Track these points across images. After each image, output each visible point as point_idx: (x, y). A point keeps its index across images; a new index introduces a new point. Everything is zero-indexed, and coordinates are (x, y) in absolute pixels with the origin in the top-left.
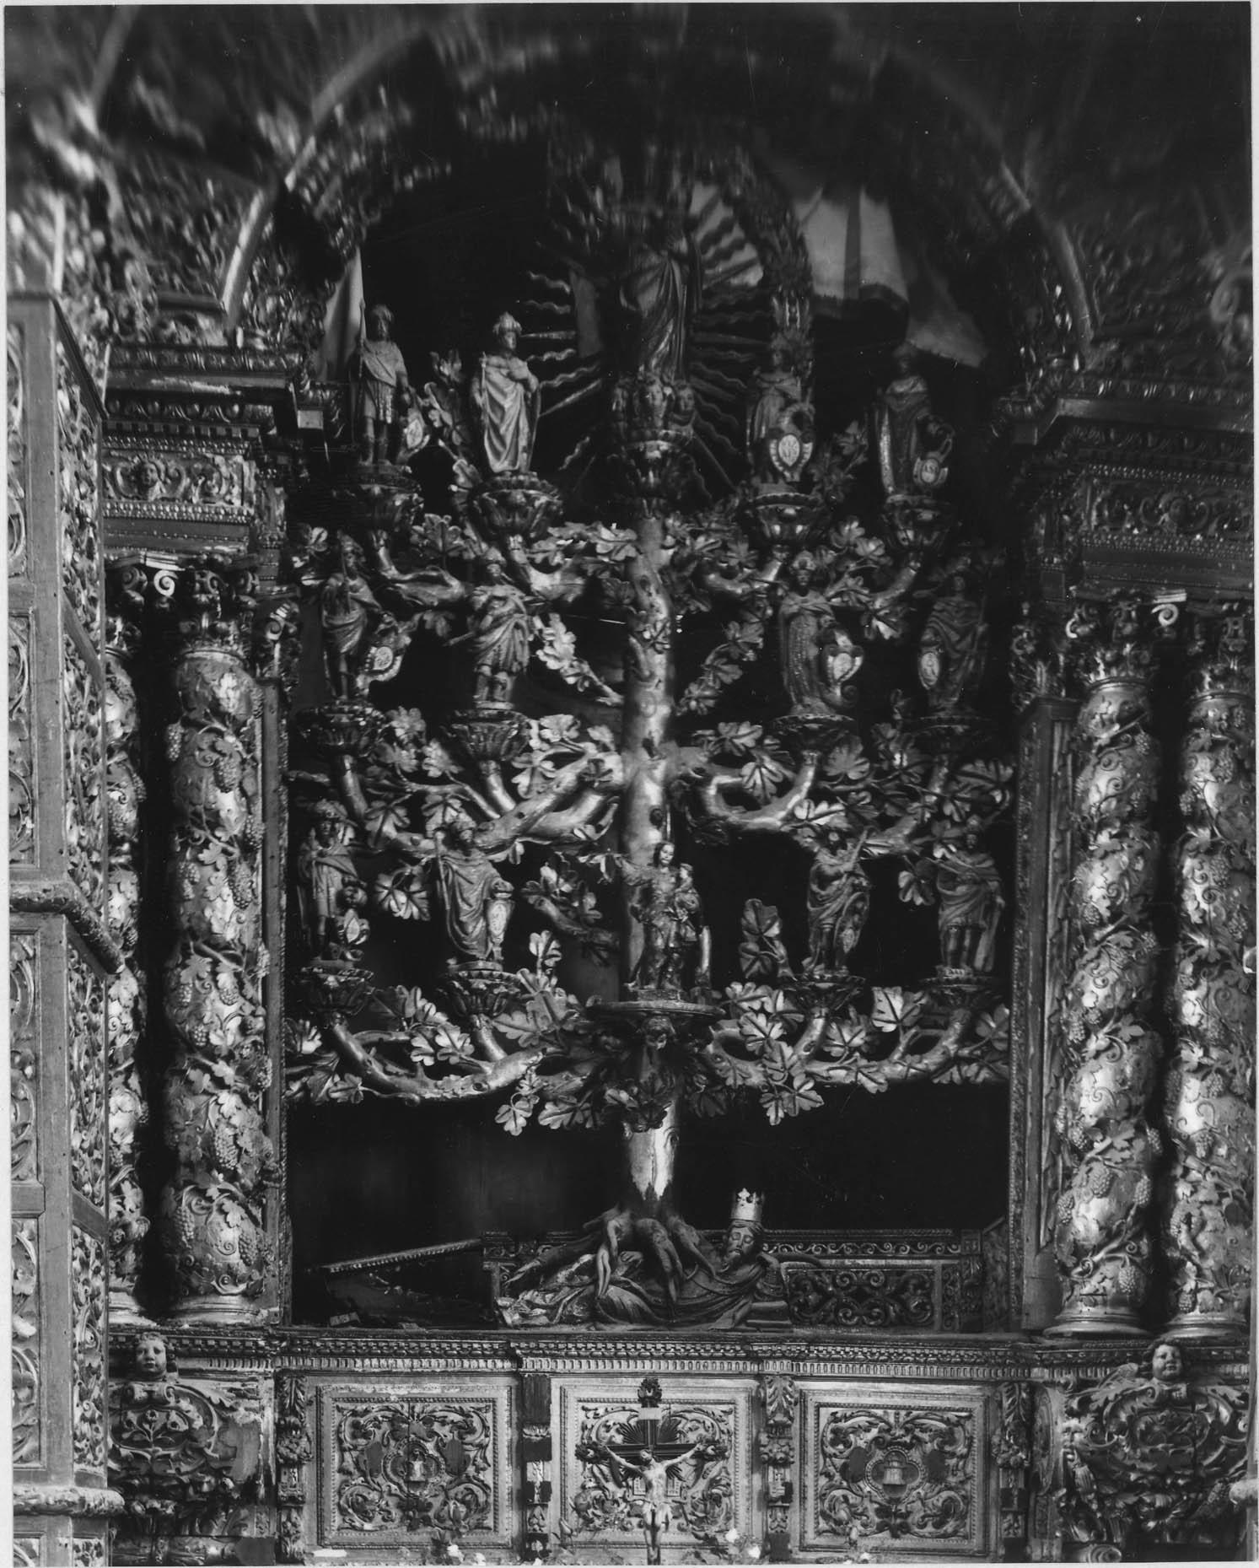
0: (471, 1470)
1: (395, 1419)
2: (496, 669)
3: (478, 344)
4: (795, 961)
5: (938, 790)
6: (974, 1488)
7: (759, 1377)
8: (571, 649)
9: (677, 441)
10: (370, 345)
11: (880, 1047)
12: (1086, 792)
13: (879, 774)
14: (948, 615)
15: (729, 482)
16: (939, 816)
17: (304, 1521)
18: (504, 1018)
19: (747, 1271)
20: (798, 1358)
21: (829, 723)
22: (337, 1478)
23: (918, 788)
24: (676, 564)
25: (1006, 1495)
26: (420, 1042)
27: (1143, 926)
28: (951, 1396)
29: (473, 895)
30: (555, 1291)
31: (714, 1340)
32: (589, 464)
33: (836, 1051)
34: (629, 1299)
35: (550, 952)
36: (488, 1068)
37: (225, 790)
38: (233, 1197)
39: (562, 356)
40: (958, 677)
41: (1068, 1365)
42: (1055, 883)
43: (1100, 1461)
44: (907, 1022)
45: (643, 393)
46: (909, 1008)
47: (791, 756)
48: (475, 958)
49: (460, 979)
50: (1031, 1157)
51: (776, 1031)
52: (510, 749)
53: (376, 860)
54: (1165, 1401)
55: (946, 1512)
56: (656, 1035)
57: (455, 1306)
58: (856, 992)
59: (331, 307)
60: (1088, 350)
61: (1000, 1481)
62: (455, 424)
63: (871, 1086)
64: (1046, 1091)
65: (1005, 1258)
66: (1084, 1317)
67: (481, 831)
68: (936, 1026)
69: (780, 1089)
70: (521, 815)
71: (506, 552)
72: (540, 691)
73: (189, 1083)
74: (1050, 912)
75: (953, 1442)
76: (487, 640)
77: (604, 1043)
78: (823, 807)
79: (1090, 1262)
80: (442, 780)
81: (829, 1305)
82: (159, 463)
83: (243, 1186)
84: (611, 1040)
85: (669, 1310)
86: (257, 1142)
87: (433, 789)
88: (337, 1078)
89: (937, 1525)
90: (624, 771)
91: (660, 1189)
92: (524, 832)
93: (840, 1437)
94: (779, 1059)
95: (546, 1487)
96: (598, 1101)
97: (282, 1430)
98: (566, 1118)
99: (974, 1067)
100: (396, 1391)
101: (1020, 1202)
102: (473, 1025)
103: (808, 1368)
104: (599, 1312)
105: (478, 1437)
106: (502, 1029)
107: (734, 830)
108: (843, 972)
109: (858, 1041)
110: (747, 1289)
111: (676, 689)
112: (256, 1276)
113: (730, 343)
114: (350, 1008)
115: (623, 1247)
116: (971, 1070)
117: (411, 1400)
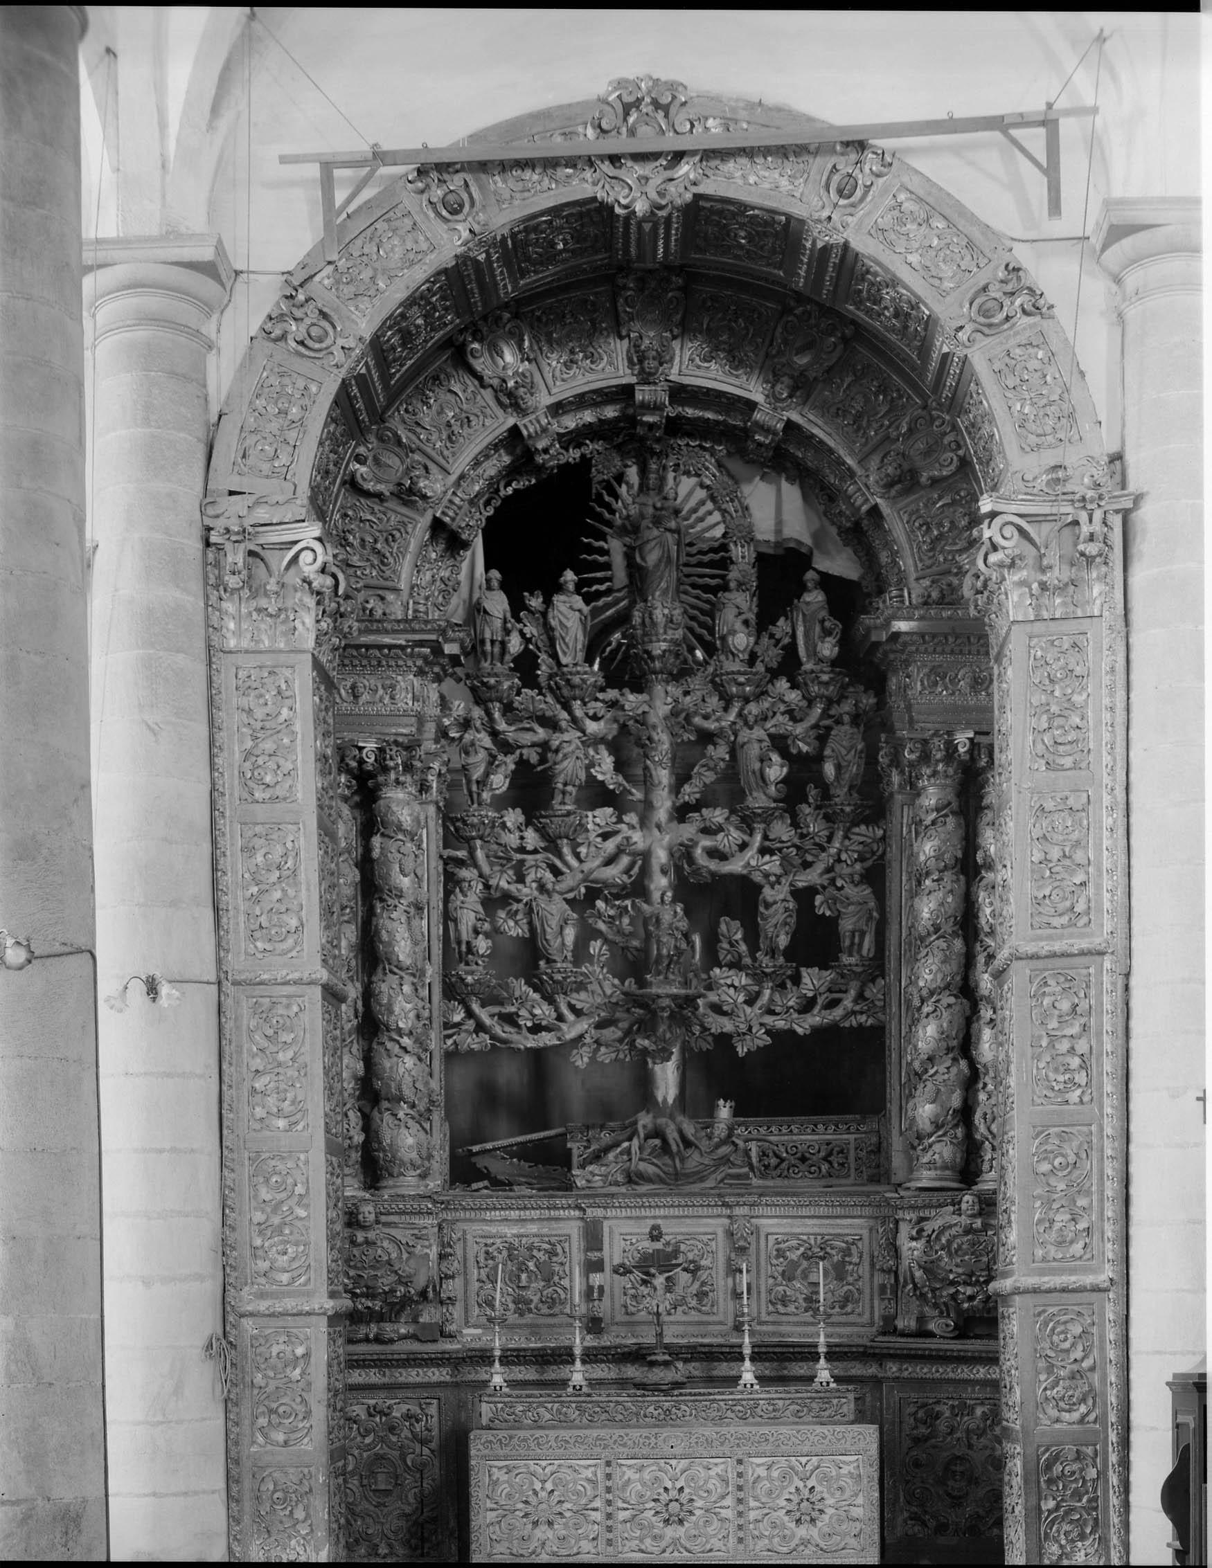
0: (556, 1278)
1: (511, 1248)
2: (565, 784)
3: (552, 588)
7: (729, 1217)
8: (611, 766)
9: (674, 642)
11: (807, 1006)
13: (802, 836)
16: (839, 861)
17: (457, 1311)
18: (575, 995)
22: (477, 1285)
24: (674, 713)
26: (523, 1012)
28: (853, 1226)
29: (554, 923)
31: (701, 1195)
33: (778, 1009)
36: (564, 1026)
41: (913, 1208)
43: (929, 1269)
45: (651, 614)
47: (747, 823)
51: (741, 999)
53: (495, 901)
54: (969, 1231)
55: (846, 1299)
57: (549, 1166)
59: (465, 566)
60: (913, 584)
61: (879, 1279)
63: (800, 1031)
66: (926, 1178)
68: (840, 991)
71: (570, 713)
72: (597, 795)
75: (850, 1255)
78: (767, 858)
79: (926, 1142)
80: (535, 851)
81: (784, 1165)
86: (427, 1083)
89: (842, 1307)
91: (670, 1101)
92: (585, 880)
95: (601, 1288)
97: (442, 1257)
98: (613, 1055)
103: (759, 1211)
104: (633, 1178)
105: (560, 1259)
107: (713, 874)
108: (781, 960)
109: (791, 1003)
110: (725, 1160)
111: (676, 789)
113: (708, 569)
115: (647, 1138)
117: (520, 1236)
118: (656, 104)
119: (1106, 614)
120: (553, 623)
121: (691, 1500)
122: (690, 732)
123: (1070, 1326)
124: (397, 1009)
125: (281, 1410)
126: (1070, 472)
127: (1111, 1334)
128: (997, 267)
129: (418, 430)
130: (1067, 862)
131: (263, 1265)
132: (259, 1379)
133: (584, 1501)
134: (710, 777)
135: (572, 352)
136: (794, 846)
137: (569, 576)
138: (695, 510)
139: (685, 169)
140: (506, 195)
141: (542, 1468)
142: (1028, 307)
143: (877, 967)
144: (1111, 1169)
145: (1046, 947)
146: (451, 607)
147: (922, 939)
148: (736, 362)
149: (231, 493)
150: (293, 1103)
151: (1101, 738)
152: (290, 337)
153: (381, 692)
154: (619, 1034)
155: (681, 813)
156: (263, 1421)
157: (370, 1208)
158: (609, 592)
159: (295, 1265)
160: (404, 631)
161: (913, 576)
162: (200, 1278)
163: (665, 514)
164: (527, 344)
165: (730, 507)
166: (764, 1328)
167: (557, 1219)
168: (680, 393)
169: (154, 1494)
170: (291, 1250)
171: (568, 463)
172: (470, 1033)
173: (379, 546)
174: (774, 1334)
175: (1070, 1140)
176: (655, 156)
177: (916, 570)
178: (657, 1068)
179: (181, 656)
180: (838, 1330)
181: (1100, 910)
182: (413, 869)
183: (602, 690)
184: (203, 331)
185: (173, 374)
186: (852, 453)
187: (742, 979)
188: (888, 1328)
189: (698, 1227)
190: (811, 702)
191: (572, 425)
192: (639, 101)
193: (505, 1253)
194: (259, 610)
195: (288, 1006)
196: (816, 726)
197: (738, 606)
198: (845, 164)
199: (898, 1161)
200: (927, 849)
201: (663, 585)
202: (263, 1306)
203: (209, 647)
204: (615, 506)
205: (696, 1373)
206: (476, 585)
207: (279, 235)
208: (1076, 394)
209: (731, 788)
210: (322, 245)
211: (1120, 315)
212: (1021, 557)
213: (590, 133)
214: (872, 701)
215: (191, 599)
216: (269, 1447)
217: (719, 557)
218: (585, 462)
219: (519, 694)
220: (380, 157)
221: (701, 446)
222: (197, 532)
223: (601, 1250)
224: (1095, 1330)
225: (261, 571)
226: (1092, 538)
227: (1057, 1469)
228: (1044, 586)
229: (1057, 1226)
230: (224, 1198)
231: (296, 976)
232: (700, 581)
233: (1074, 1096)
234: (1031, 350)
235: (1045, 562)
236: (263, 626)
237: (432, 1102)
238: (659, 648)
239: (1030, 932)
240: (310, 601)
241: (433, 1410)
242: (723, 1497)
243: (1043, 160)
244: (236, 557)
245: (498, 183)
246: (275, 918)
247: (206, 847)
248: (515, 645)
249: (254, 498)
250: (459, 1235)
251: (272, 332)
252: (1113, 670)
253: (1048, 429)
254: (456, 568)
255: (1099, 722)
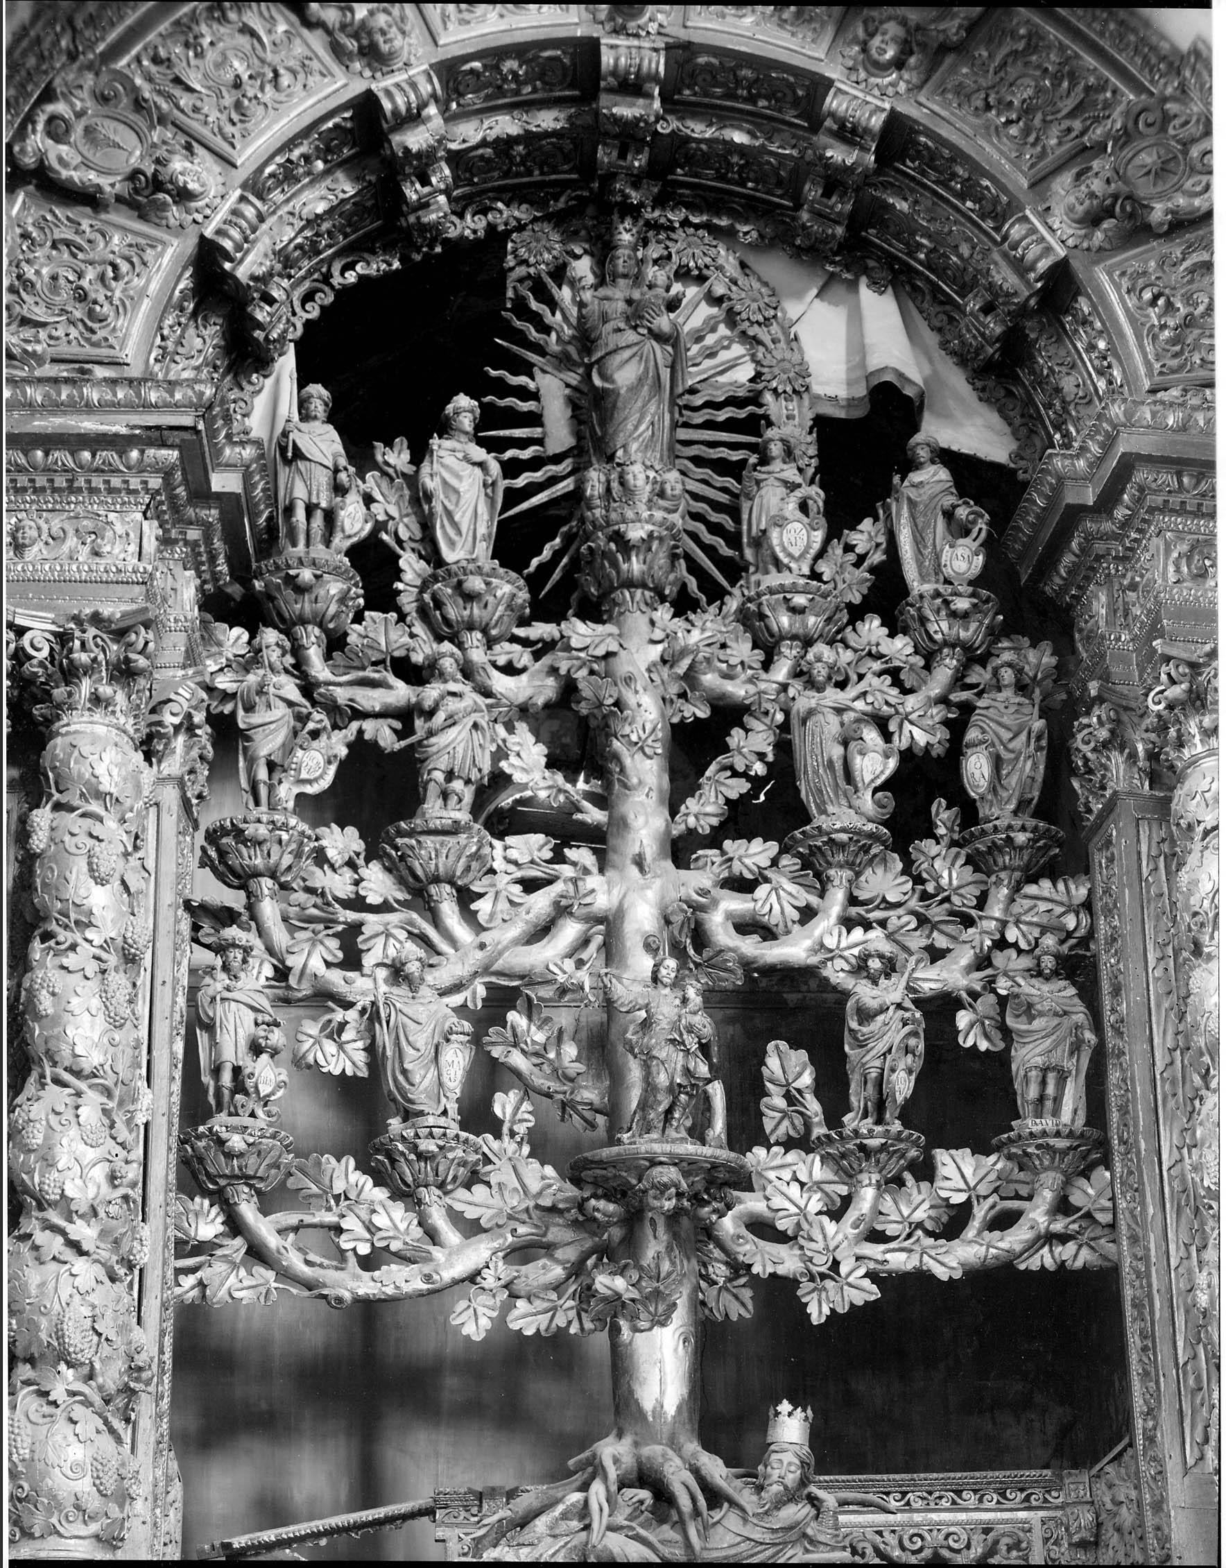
2: (450, 775)
4: (833, 1118)
5: (997, 915)
10: (303, 426)
11: (953, 1223)
12: (1195, 882)
13: (925, 896)
15: (725, 583)
16: (1001, 944)
21: (859, 832)
23: (973, 913)
29: (422, 1038)
32: (562, 566)
33: (891, 1230)
35: (519, 1116)
37: (101, 881)
38: (87, 1403)
40: (1014, 780)
42: (1158, 1006)
44: (983, 1189)
46: (982, 1172)
47: (814, 869)
48: (421, 1114)
49: (403, 1139)
50: (1163, 1350)
52: (468, 869)
58: (913, 1153)
62: (402, 517)
63: (942, 1273)
64: (1173, 1263)
65: (1133, 1494)
67: (431, 966)
69: (823, 1276)
70: (482, 946)
74: (1157, 1040)
76: (439, 741)
80: (385, 907)
82: (41, 522)
83: (101, 1388)
84: (602, 1204)
87: (370, 918)
88: (242, 1272)
90: (609, 892)
91: (670, 1408)
92: (486, 970)
94: (819, 1237)
96: (587, 1294)
98: (543, 1320)
99: (1071, 1247)
101: (1150, 1413)
102: (420, 1202)
106: (458, 1207)
107: (747, 965)
108: (897, 1126)
109: (920, 1215)
112: (115, 1512)
114: (261, 1179)
115: (622, 1485)
116: (1066, 1252)
120: (431, 484)
129: (177, 92)
143: (1093, 1148)
153: (72, 541)
154: (558, 1272)
155: (681, 850)
158: (535, 464)
171: (462, 238)
183: (524, 622)
187: (815, 1168)
190: (929, 657)
196: (943, 700)
204: (548, 318)
209: (774, 808)
214: (1049, 660)
218: (496, 239)
219: (358, 618)
221: (709, 227)
232: (715, 453)
237: (135, 1370)
248: (354, 521)
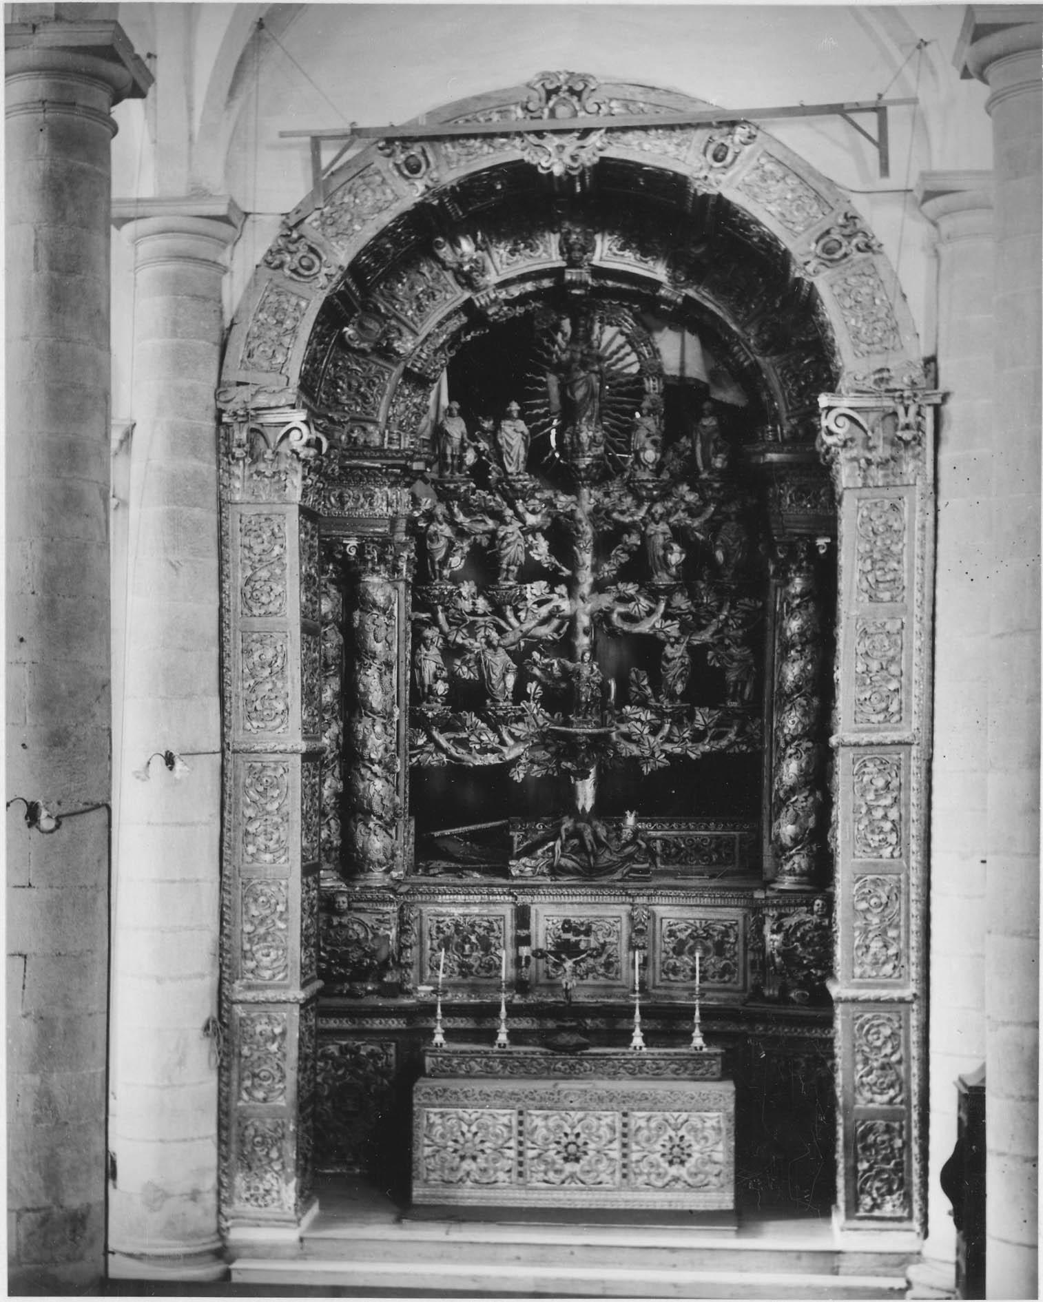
0: (493, 949)
1: (457, 925)
2: (509, 565)
3: (502, 415)
6: (739, 959)
7: (631, 904)
11: (698, 737)
13: (697, 606)
14: (729, 531)
17: (413, 974)
18: (514, 725)
19: (630, 849)
20: (649, 896)
22: (430, 952)
24: (596, 510)
25: (753, 963)
26: (473, 738)
27: (813, 694)
28: (733, 914)
29: (498, 671)
30: (536, 859)
33: (676, 739)
34: (570, 864)
36: (505, 750)
39: (542, 411)
45: (578, 436)
51: (646, 731)
53: (452, 651)
56: (581, 744)
57: (493, 858)
59: (433, 394)
60: (785, 421)
61: (750, 956)
63: (693, 756)
66: (787, 883)
72: (532, 571)
73: (362, 776)
75: (729, 936)
77: (559, 745)
78: (669, 622)
80: (484, 615)
85: (589, 871)
86: (392, 800)
87: (480, 619)
91: (588, 809)
93: (672, 934)
98: (544, 772)
100: (457, 911)
103: (656, 900)
105: (497, 934)
110: (630, 858)
111: (595, 569)
117: (465, 915)
118: (572, 91)
119: (918, 483)
120: (501, 441)
121: (586, 1144)
122: (609, 524)
123: (882, 1029)
124: (370, 743)
125: (262, 1074)
126: (892, 373)
127: (914, 1036)
128: (839, 214)
130: (884, 673)
131: (251, 964)
132: (245, 1051)
133: (500, 1142)
134: (624, 558)
135: (516, 244)
136: (690, 613)
137: (515, 407)
138: (615, 353)
139: (594, 140)
140: (455, 158)
141: (470, 1114)
142: (862, 246)
144: (915, 909)
145: (865, 738)
146: (422, 426)
147: (789, 696)
148: (645, 251)
149: (239, 384)
150: (278, 841)
151: (912, 573)
152: (286, 266)
153: (362, 500)
156: (248, 1083)
157: (344, 899)
159: (275, 965)
160: (380, 458)
161: (784, 415)
162: (202, 976)
163: (592, 358)
164: (480, 237)
165: (645, 350)
166: (658, 992)
167: (494, 903)
168: (598, 272)
169: (161, 1141)
170: (273, 954)
172: (431, 753)
173: (362, 390)
174: (665, 997)
175: (883, 885)
176: (570, 131)
177: (788, 411)
178: (579, 783)
179: (197, 510)
180: (717, 994)
181: (909, 710)
182: (385, 637)
184: (220, 261)
185: (195, 297)
186: (736, 322)
187: (648, 716)
188: (757, 994)
189: (609, 914)
190: (706, 504)
191: (517, 294)
192: (558, 89)
193: (453, 928)
194: (259, 473)
195: (275, 769)
197: (647, 425)
198: (719, 137)
199: (767, 863)
200: (794, 625)
201: (588, 413)
202: (250, 996)
203: (220, 499)
205: (602, 1026)
206: (442, 410)
207: (278, 187)
208: (898, 313)
210: (312, 196)
211: (936, 251)
212: (852, 440)
213: (520, 113)
215: (206, 465)
216: (252, 1103)
217: (633, 389)
219: (474, 493)
220: (356, 133)
222: (212, 413)
223: (528, 928)
224: (902, 1032)
225: (261, 444)
226: (907, 427)
227: (871, 1138)
228: (869, 462)
229: (872, 951)
230: (222, 914)
231: (281, 747)
233: (887, 852)
234: (864, 279)
235: (871, 444)
236: (261, 485)
237: (396, 814)
238: (585, 462)
239: (854, 726)
240: (299, 467)
241: (392, 1051)
242: (611, 1142)
243: (875, 136)
244: (241, 435)
245: (448, 148)
246: (267, 703)
247: (215, 651)
249: (257, 388)
250: (417, 914)
251: (272, 261)
252: (923, 527)
253: (876, 339)
254: (426, 396)
255: (912, 565)
